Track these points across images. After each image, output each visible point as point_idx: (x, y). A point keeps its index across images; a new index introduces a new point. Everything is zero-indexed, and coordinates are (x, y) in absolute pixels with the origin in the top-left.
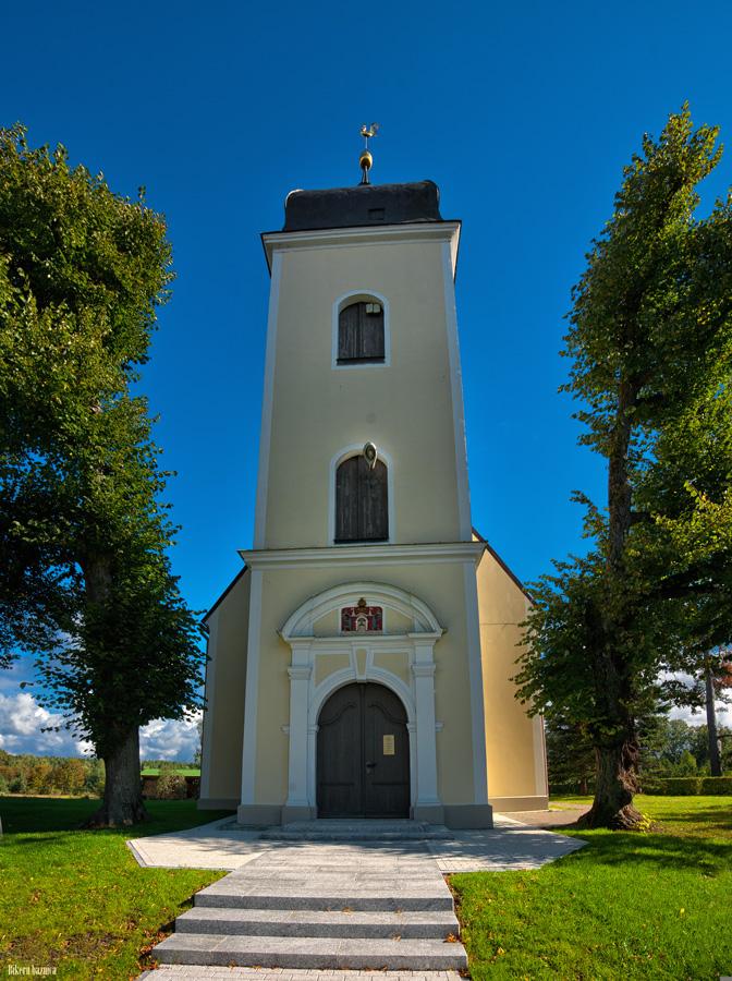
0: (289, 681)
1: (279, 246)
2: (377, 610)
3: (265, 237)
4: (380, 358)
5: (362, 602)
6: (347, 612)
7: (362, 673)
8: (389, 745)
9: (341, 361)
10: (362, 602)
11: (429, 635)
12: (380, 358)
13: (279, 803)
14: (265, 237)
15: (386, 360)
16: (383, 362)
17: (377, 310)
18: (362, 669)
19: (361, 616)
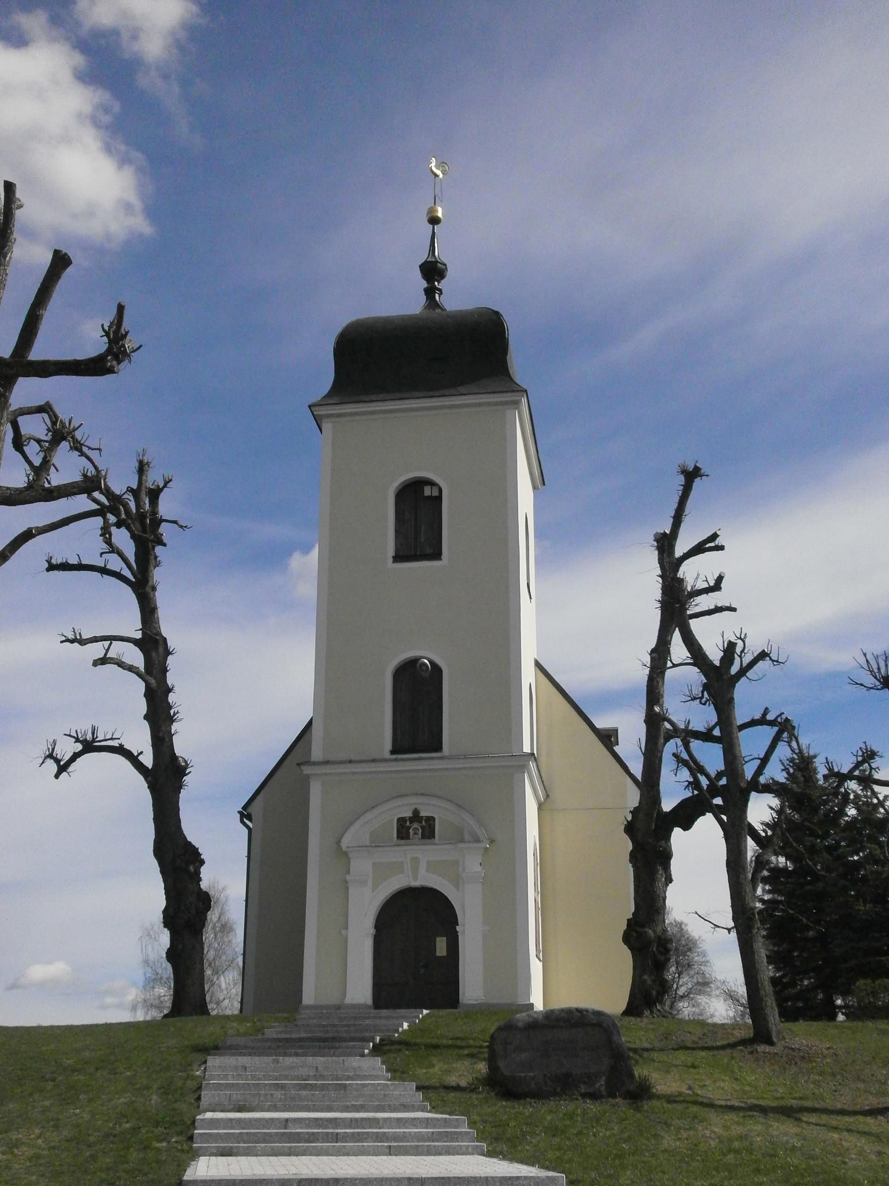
4: (436, 555)
5: (416, 812)
6: (401, 821)
8: (441, 947)
9: (399, 558)
10: (416, 812)
12: (436, 555)
17: (436, 493)
18: (416, 879)
19: (416, 825)
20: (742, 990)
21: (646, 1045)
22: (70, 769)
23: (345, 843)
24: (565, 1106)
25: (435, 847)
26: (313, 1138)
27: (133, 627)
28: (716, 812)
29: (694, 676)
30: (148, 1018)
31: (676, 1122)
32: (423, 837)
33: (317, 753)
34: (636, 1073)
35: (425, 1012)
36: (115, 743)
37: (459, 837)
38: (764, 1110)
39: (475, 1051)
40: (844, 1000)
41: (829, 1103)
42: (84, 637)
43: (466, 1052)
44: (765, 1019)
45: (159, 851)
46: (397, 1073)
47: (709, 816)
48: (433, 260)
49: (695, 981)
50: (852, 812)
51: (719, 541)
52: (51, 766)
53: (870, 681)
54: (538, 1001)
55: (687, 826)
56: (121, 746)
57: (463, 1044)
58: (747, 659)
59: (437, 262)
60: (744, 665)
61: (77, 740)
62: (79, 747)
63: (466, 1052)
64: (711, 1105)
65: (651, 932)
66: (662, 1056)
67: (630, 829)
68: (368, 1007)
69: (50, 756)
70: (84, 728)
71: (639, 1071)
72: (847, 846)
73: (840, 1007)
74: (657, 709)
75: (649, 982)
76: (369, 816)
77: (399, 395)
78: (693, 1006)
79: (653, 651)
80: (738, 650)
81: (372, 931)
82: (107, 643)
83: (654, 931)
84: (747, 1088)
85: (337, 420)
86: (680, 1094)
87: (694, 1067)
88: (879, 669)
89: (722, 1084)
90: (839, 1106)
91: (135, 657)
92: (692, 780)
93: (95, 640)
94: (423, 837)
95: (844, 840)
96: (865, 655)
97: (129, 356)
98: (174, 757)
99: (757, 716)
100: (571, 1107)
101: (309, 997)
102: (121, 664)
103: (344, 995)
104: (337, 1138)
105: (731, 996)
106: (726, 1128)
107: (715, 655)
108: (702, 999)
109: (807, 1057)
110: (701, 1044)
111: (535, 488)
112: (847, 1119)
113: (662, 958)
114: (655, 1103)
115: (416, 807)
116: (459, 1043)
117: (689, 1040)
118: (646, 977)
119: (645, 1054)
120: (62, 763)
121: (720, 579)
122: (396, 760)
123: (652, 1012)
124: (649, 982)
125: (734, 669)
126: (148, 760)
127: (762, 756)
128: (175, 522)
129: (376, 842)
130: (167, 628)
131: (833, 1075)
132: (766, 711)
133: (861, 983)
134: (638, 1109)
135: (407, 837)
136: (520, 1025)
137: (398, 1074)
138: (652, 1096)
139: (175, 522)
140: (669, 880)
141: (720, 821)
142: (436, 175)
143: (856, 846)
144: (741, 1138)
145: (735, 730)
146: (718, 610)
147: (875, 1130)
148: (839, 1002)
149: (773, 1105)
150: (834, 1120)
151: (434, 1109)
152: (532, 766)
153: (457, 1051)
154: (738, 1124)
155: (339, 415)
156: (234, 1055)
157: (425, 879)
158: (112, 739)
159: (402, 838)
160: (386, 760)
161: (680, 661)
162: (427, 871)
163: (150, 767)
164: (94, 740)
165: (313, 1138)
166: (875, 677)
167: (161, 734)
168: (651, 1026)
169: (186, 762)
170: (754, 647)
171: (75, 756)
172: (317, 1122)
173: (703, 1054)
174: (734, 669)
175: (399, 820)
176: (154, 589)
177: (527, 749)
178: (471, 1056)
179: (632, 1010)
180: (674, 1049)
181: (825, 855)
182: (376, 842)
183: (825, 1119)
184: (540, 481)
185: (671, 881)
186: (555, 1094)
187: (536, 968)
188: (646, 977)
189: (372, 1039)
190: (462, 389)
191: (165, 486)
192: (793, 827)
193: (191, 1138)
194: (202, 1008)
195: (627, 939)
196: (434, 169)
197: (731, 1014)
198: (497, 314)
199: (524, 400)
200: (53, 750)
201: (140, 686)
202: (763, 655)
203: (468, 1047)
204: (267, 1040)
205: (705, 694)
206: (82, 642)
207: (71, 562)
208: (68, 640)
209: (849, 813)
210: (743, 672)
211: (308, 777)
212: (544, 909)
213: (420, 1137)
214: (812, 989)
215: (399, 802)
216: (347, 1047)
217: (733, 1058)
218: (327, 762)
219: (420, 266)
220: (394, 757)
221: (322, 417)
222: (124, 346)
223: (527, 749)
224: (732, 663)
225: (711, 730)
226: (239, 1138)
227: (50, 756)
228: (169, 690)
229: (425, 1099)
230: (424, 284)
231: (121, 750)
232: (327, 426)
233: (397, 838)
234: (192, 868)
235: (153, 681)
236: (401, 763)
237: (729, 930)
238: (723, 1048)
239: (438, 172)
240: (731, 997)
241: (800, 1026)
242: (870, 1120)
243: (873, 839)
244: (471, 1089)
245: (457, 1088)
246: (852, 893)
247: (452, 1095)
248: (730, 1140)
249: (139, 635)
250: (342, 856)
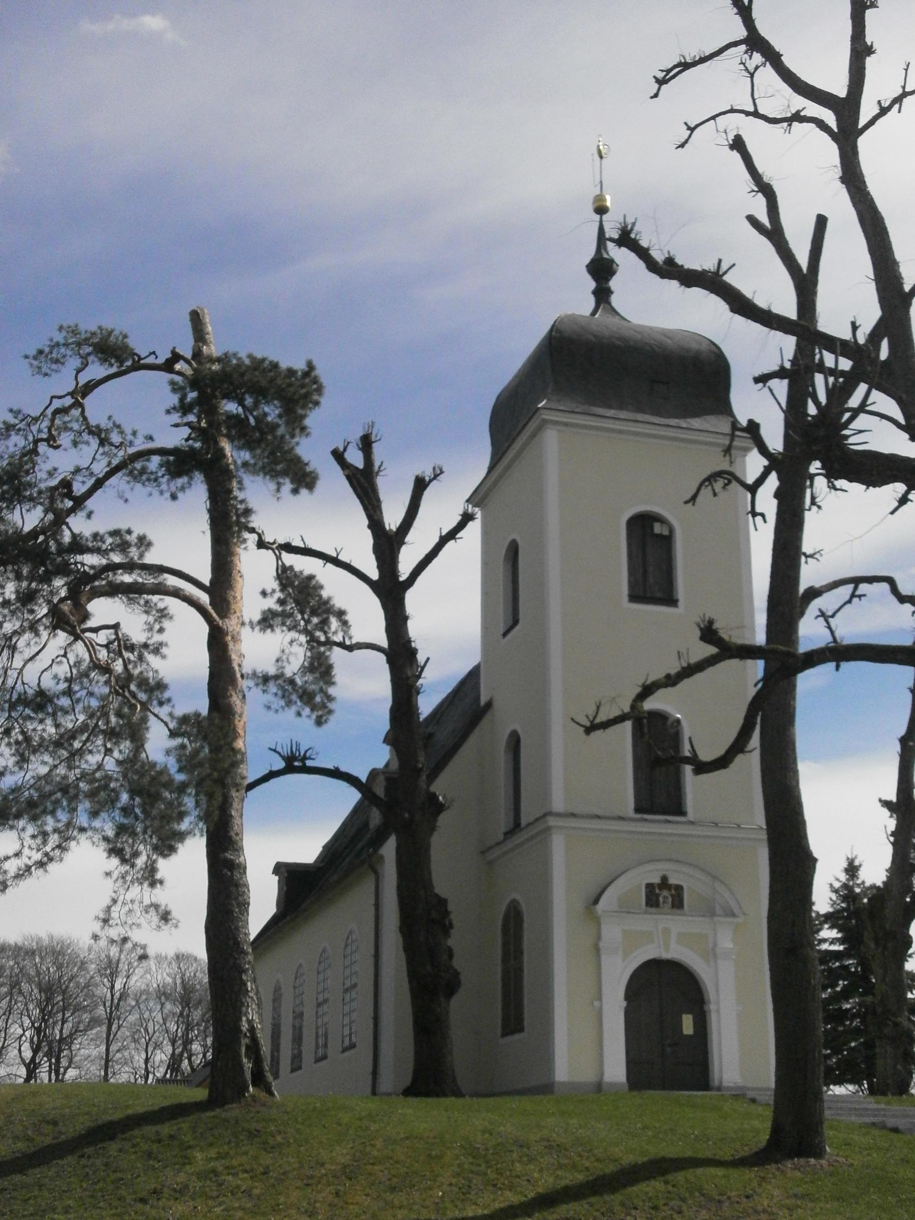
4: (634, 597)
5: (664, 879)
8: (688, 1025)
10: (664, 879)
12: (634, 597)
18: (667, 950)
19: (665, 893)
25: (685, 918)
32: (673, 906)
85: (564, 428)
94: (673, 906)
103: (602, 1074)
115: (665, 873)
135: (657, 905)
155: (566, 425)
157: (675, 952)
159: (652, 906)
182: (625, 908)
207: (294, 544)
215: (650, 867)
220: (639, 816)
230: (592, 285)
236: (671, 826)
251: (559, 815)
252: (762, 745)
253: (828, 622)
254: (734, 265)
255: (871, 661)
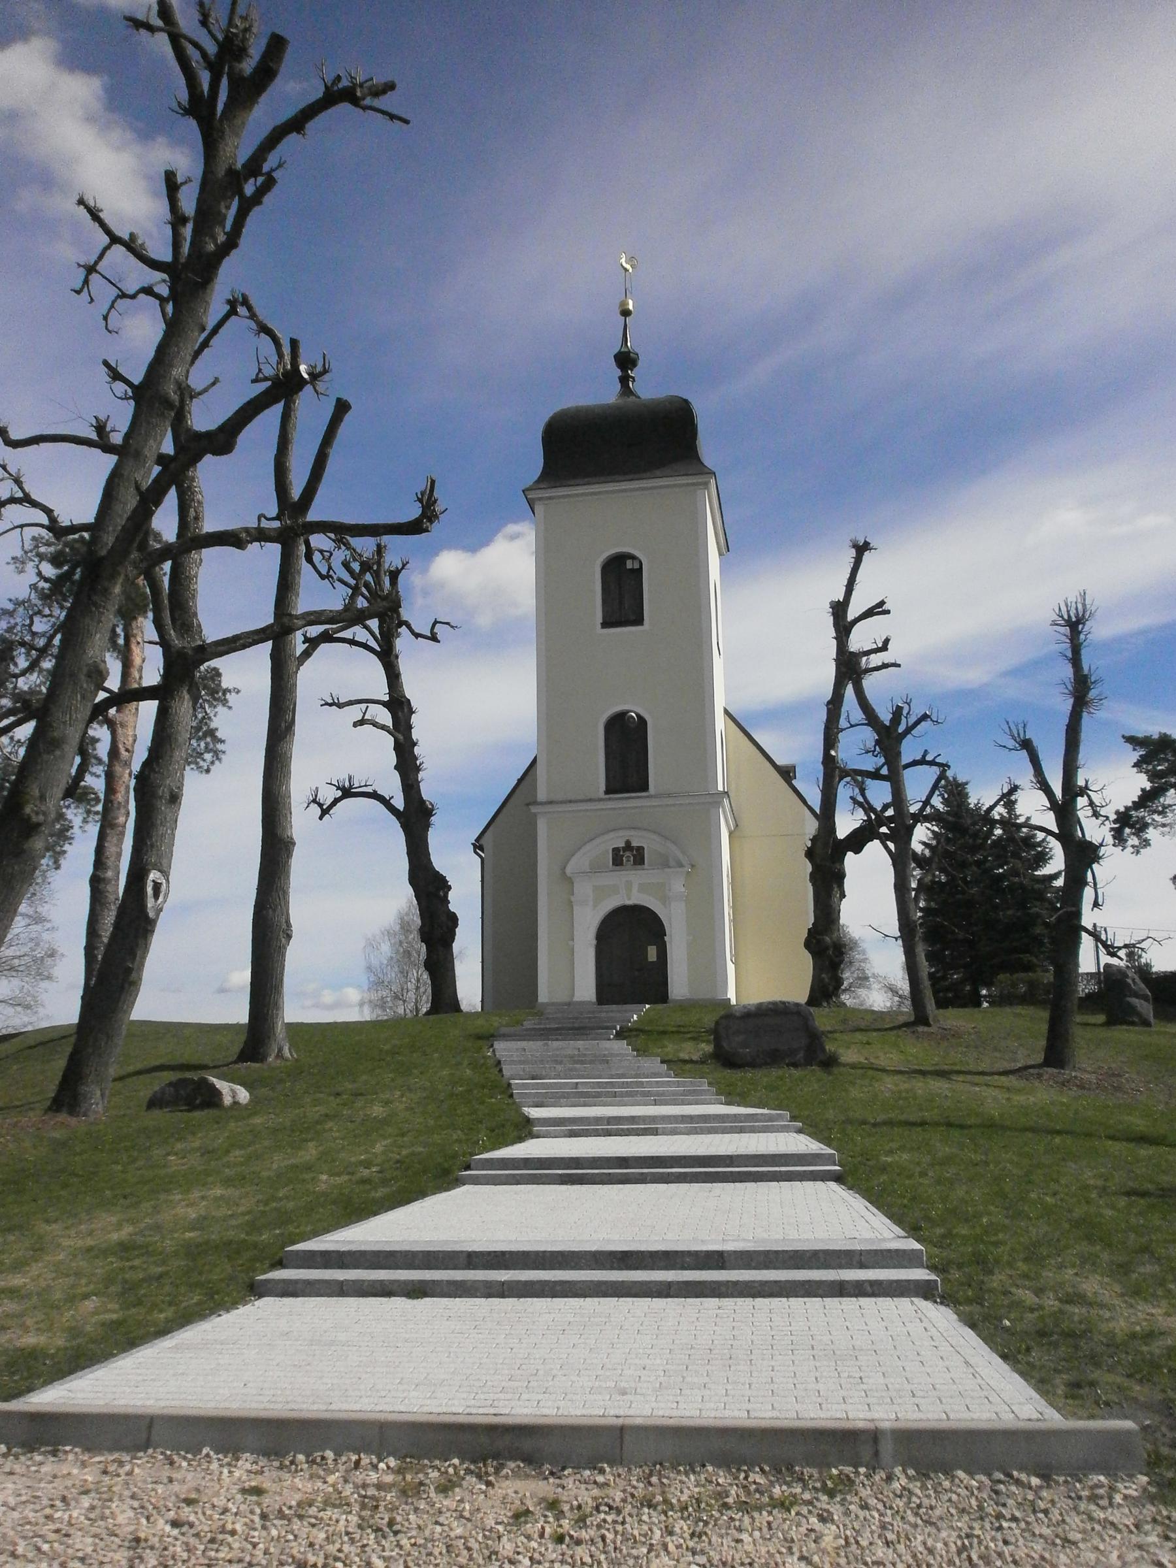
0: (570, 904)
1: (540, 499)
2: (640, 850)
3: (527, 493)
4: (639, 621)
5: (628, 843)
6: (616, 851)
7: (629, 899)
8: (652, 953)
9: (606, 624)
10: (628, 843)
11: (680, 869)
12: (639, 621)
13: (566, 999)
14: (527, 493)
15: (645, 622)
16: (642, 624)
17: (637, 566)
18: (629, 899)
19: (628, 854)
20: (904, 986)
21: (829, 1028)
22: (331, 812)
23: (568, 871)
24: (775, 1072)
25: (646, 872)
26: (598, 1095)
27: (381, 691)
28: (883, 839)
29: (868, 736)
30: (374, 1017)
31: (858, 1081)
32: (635, 863)
33: (542, 795)
34: (827, 1047)
35: (647, 1006)
36: (369, 790)
37: (664, 863)
38: (923, 1073)
39: (695, 1035)
40: (988, 990)
41: (971, 1067)
42: (341, 701)
43: (689, 1036)
44: (924, 1007)
45: (413, 879)
46: (641, 1051)
47: (877, 842)
48: (626, 350)
49: (855, 975)
50: (998, 832)
51: (885, 607)
52: (316, 810)
53: (1011, 743)
54: (732, 995)
55: (858, 851)
56: (375, 792)
57: (686, 1030)
58: (912, 720)
59: (629, 352)
60: (910, 724)
61: (338, 788)
62: (339, 793)
63: (689, 1036)
64: (884, 1070)
65: (827, 939)
66: (845, 1037)
67: (810, 854)
68: (594, 1004)
69: (314, 801)
70: (342, 776)
71: (830, 1047)
72: (994, 861)
73: (985, 996)
74: (833, 753)
75: (827, 980)
76: (588, 847)
77: (602, 479)
78: (854, 998)
79: (829, 703)
80: (905, 712)
81: (594, 942)
82: (363, 706)
83: (831, 939)
84: (911, 1058)
86: (860, 1063)
87: (868, 1043)
88: (1019, 734)
89: (891, 1056)
90: (981, 1069)
91: (384, 716)
92: (866, 818)
93: (351, 703)
94: (635, 863)
95: (991, 856)
96: (1008, 723)
97: (438, 518)
98: (423, 802)
99: (918, 757)
100: (780, 1072)
101: (543, 997)
102: (375, 724)
104: (615, 1095)
105: (892, 990)
106: (896, 1085)
107: (885, 717)
108: (862, 992)
109: (956, 1035)
110: (873, 1027)
111: (720, 554)
112: (986, 1078)
113: (837, 960)
114: (842, 1069)
116: (682, 1029)
117: (863, 1025)
118: (823, 976)
119: (829, 1035)
120: (325, 807)
121: (887, 641)
122: (610, 799)
123: (829, 1003)
124: (827, 980)
125: (901, 729)
126: (399, 803)
127: (923, 799)
128: (448, 624)
129: (596, 869)
130: (411, 689)
131: (976, 1047)
132: (926, 752)
133: (1001, 977)
134: (830, 1074)
135: (621, 864)
136: (738, 1014)
137: (641, 1053)
138: (839, 1064)
139: (448, 624)
140: (843, 896)
141: (886, 848)
142: (626, 270)
143: (1001, 860)
144: (907, 1091)
145: (901, 768)
146: (885, 666)
147: (1007, 1084)
148: (984, 992)
149: (931, 1069)
150: (977, 1079)
151: (676, 1076)
152: (726, 802)
153: (681, 1035)
154: (904, 1082)
155: (550, 498)
156: (514, 1040)
158: (366, 786)
160: (600, 800)
161: (857, 722)
162: (638, 892)
163: (402, 810)
164: (351, 787)
165: (598, 1095)
166: (1015, 740)
167: (410, 782)
168: (831, 1014)
169: (431, 803)
170: (917, 711)
171: (336, 801)
172: (599, 1085)
173: (875, 1034)
174: (901, 729)
175: (614, 849)
176: (397, 657)
177: (720, 788)
178: (693, 1039)
179: (813, 1001)
180: (851, 1031)
181: (975, 869)
182: (596, 869)
183: (969, 1077)
184: (725, 548)
185: (844, 896)
186: (766, 1064)
187: (731, 968)
188: (823, 976)
189: (615, 1029)
190: (658, 473)
191: (403, 568)
192: (947, 855)
193: (511, 1096)
194: (455, 1006)
195: (808, 945)
196: (624, 264)
197: (888, 1004)
198: (686, 401)
199: (713, 481)
200: (316, 796)
201: (390, 741)
202: (925, 717)
203: (689, 1032)
204: (527, 1030)
205: (877, 747)
206: (340, 706)
208: (327, 704)
209: (996, 833)
210: (909, 730)
211: (535, 815)
212: (735, 921)
213: (674, 1094)
214: (962, 982)
215: (612, 835)
216: (597, 1034)
217: (899, 1036)
218: (551, 803)
219: (615, 356)
220: (607, 796)
221: (533, 499)
222: (434, 509)
223: (720, 788)
224: (899, 723)
225: (878, 770)
226: (545, 1095)
227: (314, 801)
228: (415, 744)
229: (669, 1069)
230: (619, 373)
231: (374, 795)
232: (539, 508)
233: (613, 864)
234: (442, 894)
235: (401, 737)
237: (896, 939)
238: (891, 1029)
239: (628, 267)
240: (891, 990)
241: (951, 1012)
242: (1003, 1078)
243: (1016, 855)
244: (702, 1062)
245: (691, 1061)
246: (968, 988)
247: (688, 1066)
248: (900, 1092)
249: (386, 698)
250: (567, 881)
251: (542, 804)
252: (231, 1081)
253: (108, 232)
254: (406, 122)
255: (313, 467)
